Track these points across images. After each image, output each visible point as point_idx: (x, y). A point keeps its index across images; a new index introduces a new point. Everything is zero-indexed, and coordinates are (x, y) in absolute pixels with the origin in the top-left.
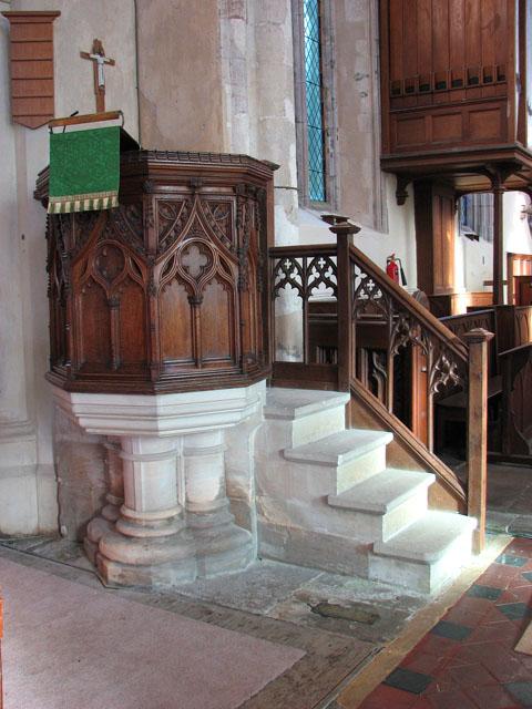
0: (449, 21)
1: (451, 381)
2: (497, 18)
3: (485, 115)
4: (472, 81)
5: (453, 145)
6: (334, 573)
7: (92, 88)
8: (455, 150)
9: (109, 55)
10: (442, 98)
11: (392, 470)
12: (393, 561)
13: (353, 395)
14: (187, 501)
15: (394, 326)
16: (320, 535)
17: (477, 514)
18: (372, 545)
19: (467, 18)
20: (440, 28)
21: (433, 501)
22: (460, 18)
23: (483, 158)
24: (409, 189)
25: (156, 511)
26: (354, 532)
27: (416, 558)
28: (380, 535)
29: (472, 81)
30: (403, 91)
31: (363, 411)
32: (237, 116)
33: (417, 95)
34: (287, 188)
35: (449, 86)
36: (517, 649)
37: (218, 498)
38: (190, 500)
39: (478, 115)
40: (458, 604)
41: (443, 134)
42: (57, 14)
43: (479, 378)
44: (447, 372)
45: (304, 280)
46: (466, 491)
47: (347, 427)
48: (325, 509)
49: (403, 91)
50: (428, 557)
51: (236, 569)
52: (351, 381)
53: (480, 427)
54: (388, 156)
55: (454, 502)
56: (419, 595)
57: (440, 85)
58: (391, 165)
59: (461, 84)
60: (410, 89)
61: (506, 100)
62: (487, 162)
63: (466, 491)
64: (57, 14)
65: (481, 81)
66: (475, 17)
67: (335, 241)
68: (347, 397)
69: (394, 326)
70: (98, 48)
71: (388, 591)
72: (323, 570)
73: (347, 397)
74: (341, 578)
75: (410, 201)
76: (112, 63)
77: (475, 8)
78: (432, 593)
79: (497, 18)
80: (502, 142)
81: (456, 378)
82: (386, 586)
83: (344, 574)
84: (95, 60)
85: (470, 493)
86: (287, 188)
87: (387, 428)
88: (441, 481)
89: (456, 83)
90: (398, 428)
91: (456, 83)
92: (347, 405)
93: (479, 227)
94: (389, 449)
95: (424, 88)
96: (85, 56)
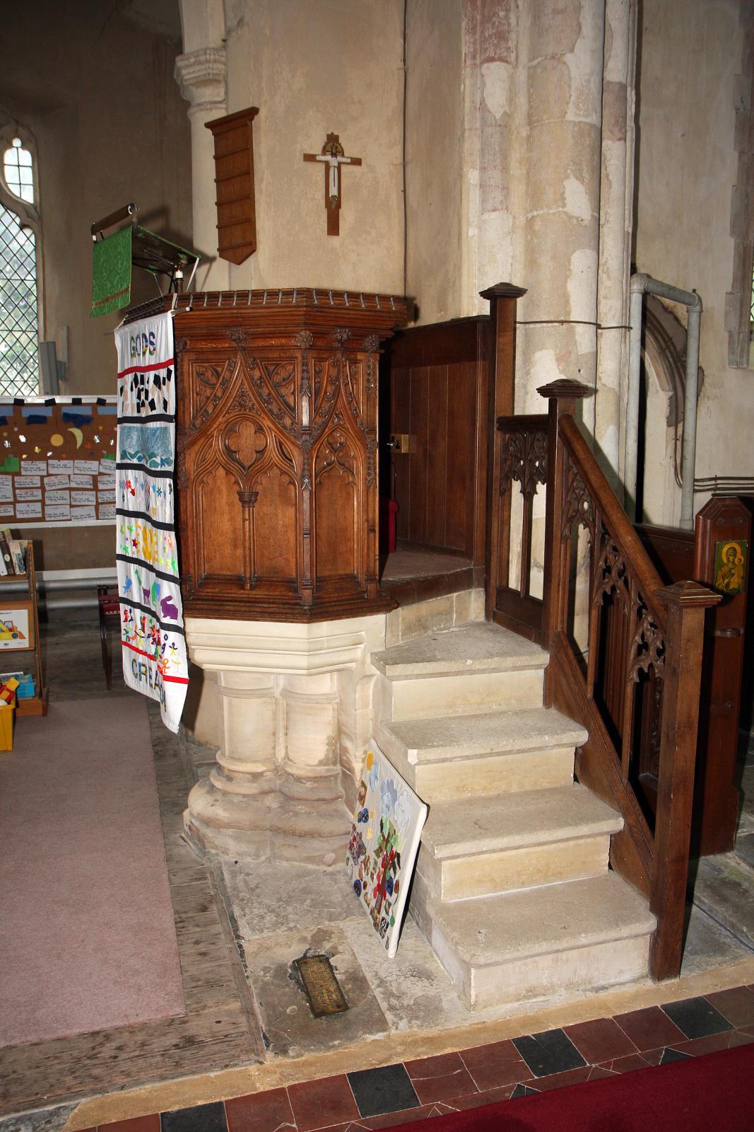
7: (323, 202)
9: (350, 150)
14: (287, 757)
25: (240, 760)
32: (486, 216)
34: (562, 322)
37: (321, 763)
38: (291, 755)
42: (253, 112)
45: (21, 307)
51: (318, 864)
64: (253, 112)
70: (333, 145)
76: (357, 162)
84: (327, 164)
86: (562, 322)
96: (310, 158)
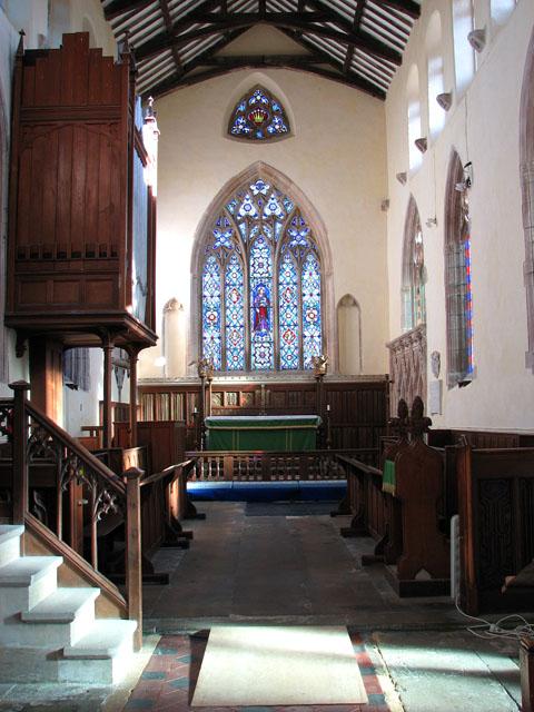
0: (71, 203)
1: (111, 510)
2: (112, 205)
3: (99, 284)
4: (90, 254)
5: (70, 308)
6: (25, 683)
8: (74, 312)
10: (62, 266)
11: (62, 589)
12: (80, 662)
13: (27, 528)
15: (63, 467)
16: (11, 650)
17: (136, 618)
18: (62, 650)
19: (86, 200)
20: (63, 207)
21: (100, 612)
22: (81, 201)
23: (98, 320)
24: (26, 344)
26: (47, 641)
27: (98, 656)
28: (69, 640)
29: (90, 254)
30: (28, 257)
31: (35, 541)
33: (40, 261)
35: (69, 256)
36: (193, 704)
39: (94, 284)
40: (138, 686)
41: (63, 296)
43: (135, 506)
44: (108, 502)
46: (127, 600)
47: (21, 555)
48: (21, 626)
49: (28, 257)
50: (111, 652)
52: (25, 516)
53: (135, 545)
54: (11, 313)
55: (117, 611)
56: (104, 686)
57: (61, 256)
58: (16, 322)
59: (80, 256)
60: (34, 255)
61: (118, 273)
62: (102, 324)
63: (127, 600)
65: (97, 255)
66: (93, 203)
67: (13, 396)
68: (22, 529)
69: (63, 467)
71: (76, 688)
72: (13, 682)
73: (22, 529)
74: (33, 686)
75: (26, 354)
77: (94, 195)
78: (114, 683)
79: (112, 205)
80: (114, 308)
81: (115, 508)
82: (75, 685)
83: (34, 682)
85: (130, 600)
87: (57, 552)
88: (105, 593)
89: (76, 255)
90: (66, 551)
91: (76, 255)
92: (21, 537)
93: (76, 378)
94: (59, 570)
95: (47, 256)
